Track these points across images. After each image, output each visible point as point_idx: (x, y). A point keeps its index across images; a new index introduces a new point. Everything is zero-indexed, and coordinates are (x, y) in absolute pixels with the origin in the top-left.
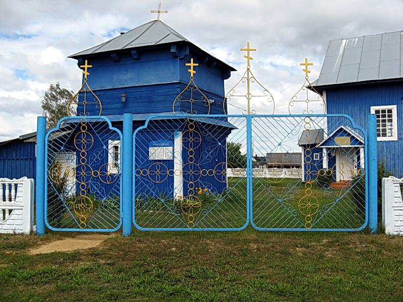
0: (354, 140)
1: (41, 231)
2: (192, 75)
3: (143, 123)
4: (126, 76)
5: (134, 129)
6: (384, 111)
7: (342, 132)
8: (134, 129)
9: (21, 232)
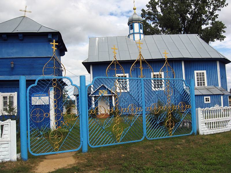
0: (110, 92)
1: (25, 156)
2: (54, 51)
3: (34, 81)
4: (13, 50)
5: (27, 87)
6: (200, 73)
7: (103, 88)
8: (27, 87)
9: (9, 160)
